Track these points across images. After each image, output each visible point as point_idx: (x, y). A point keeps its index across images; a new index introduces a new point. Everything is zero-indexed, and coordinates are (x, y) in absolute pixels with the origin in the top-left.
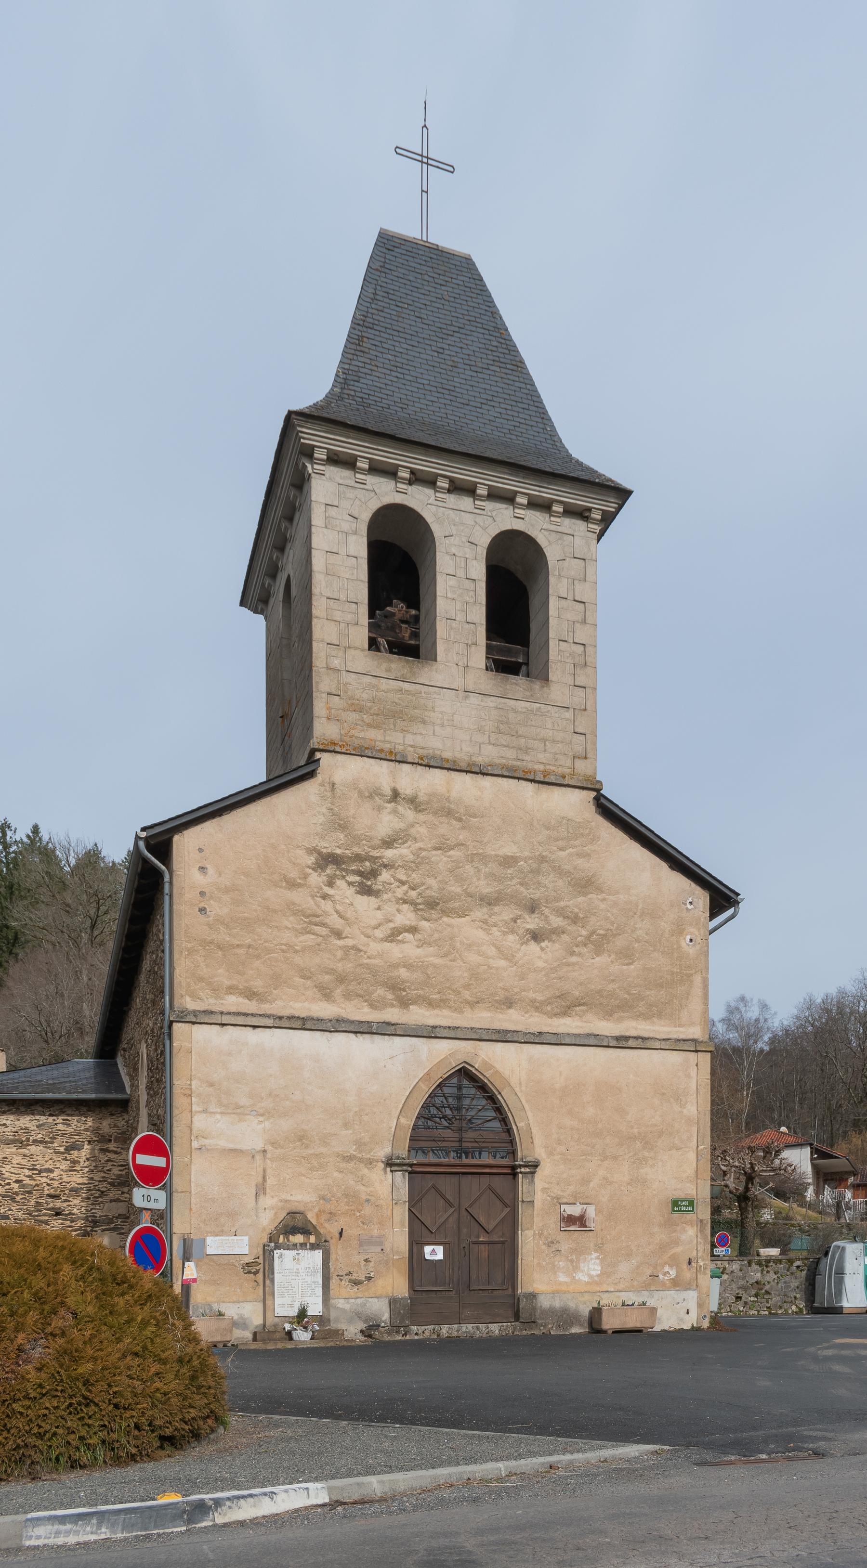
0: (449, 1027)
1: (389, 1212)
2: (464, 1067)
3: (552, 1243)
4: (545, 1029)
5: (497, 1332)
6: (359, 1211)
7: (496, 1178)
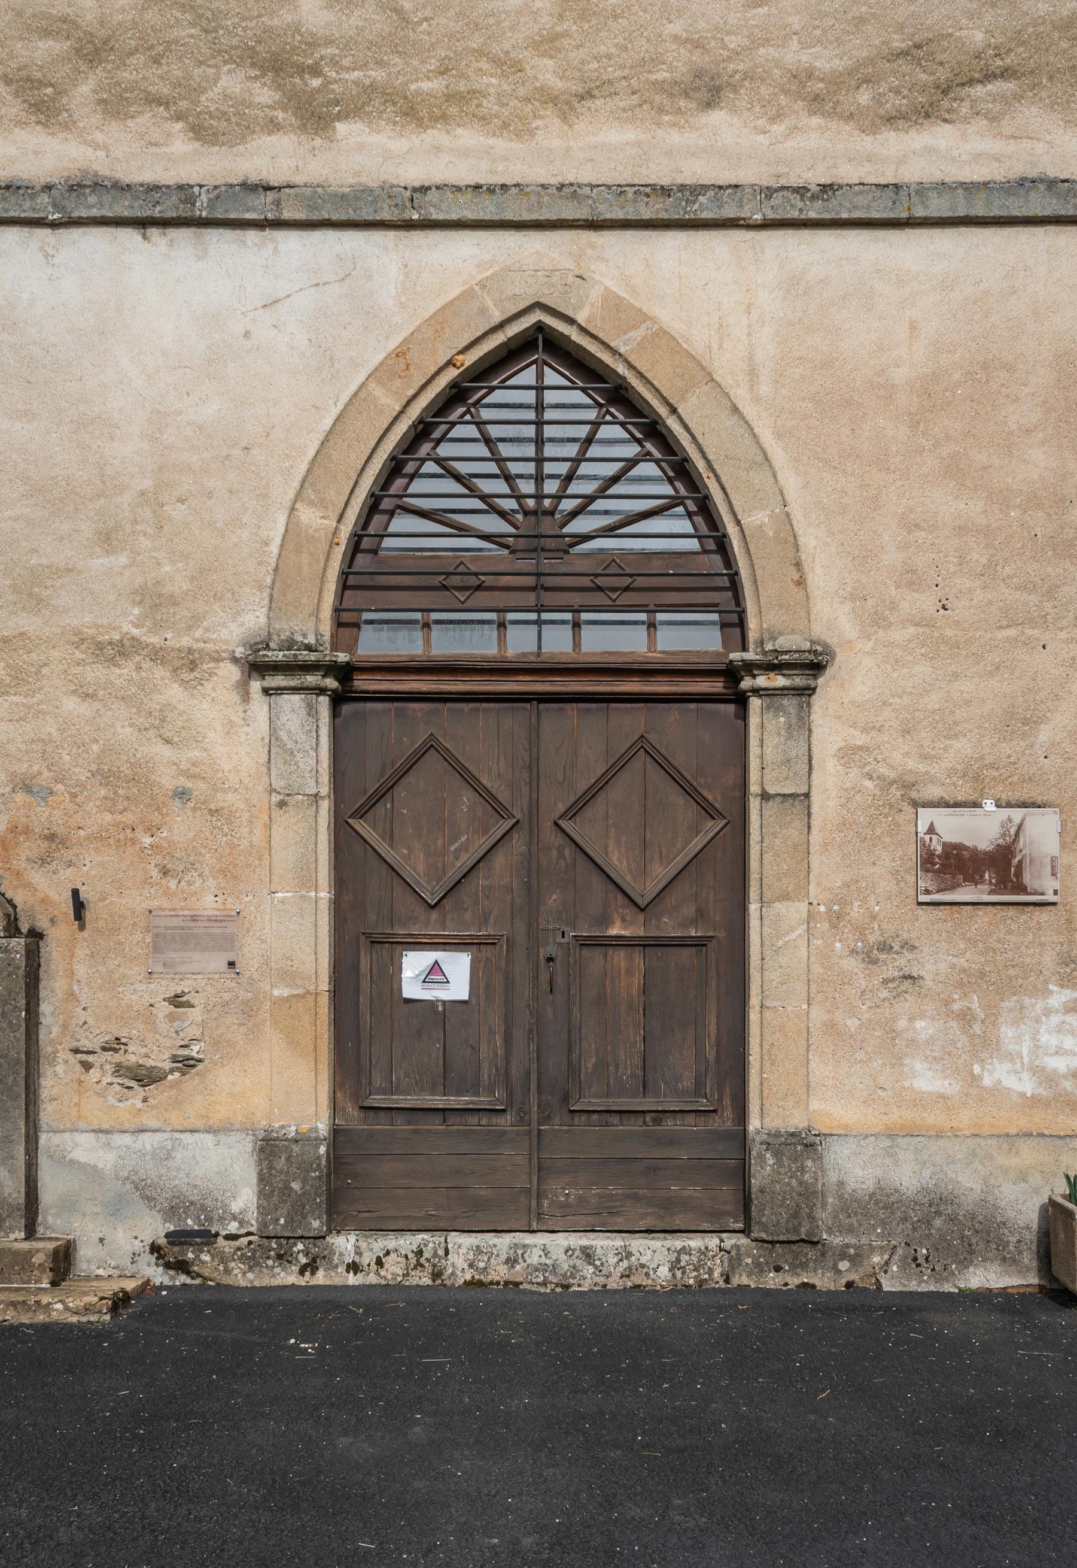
0: (477, 187)
1: (259, 835)
2: (540, 327)
3: (885, 947)
4: (848, 173)
5: (664, 1272)
6: (151, 831)
7: (673, 713)
